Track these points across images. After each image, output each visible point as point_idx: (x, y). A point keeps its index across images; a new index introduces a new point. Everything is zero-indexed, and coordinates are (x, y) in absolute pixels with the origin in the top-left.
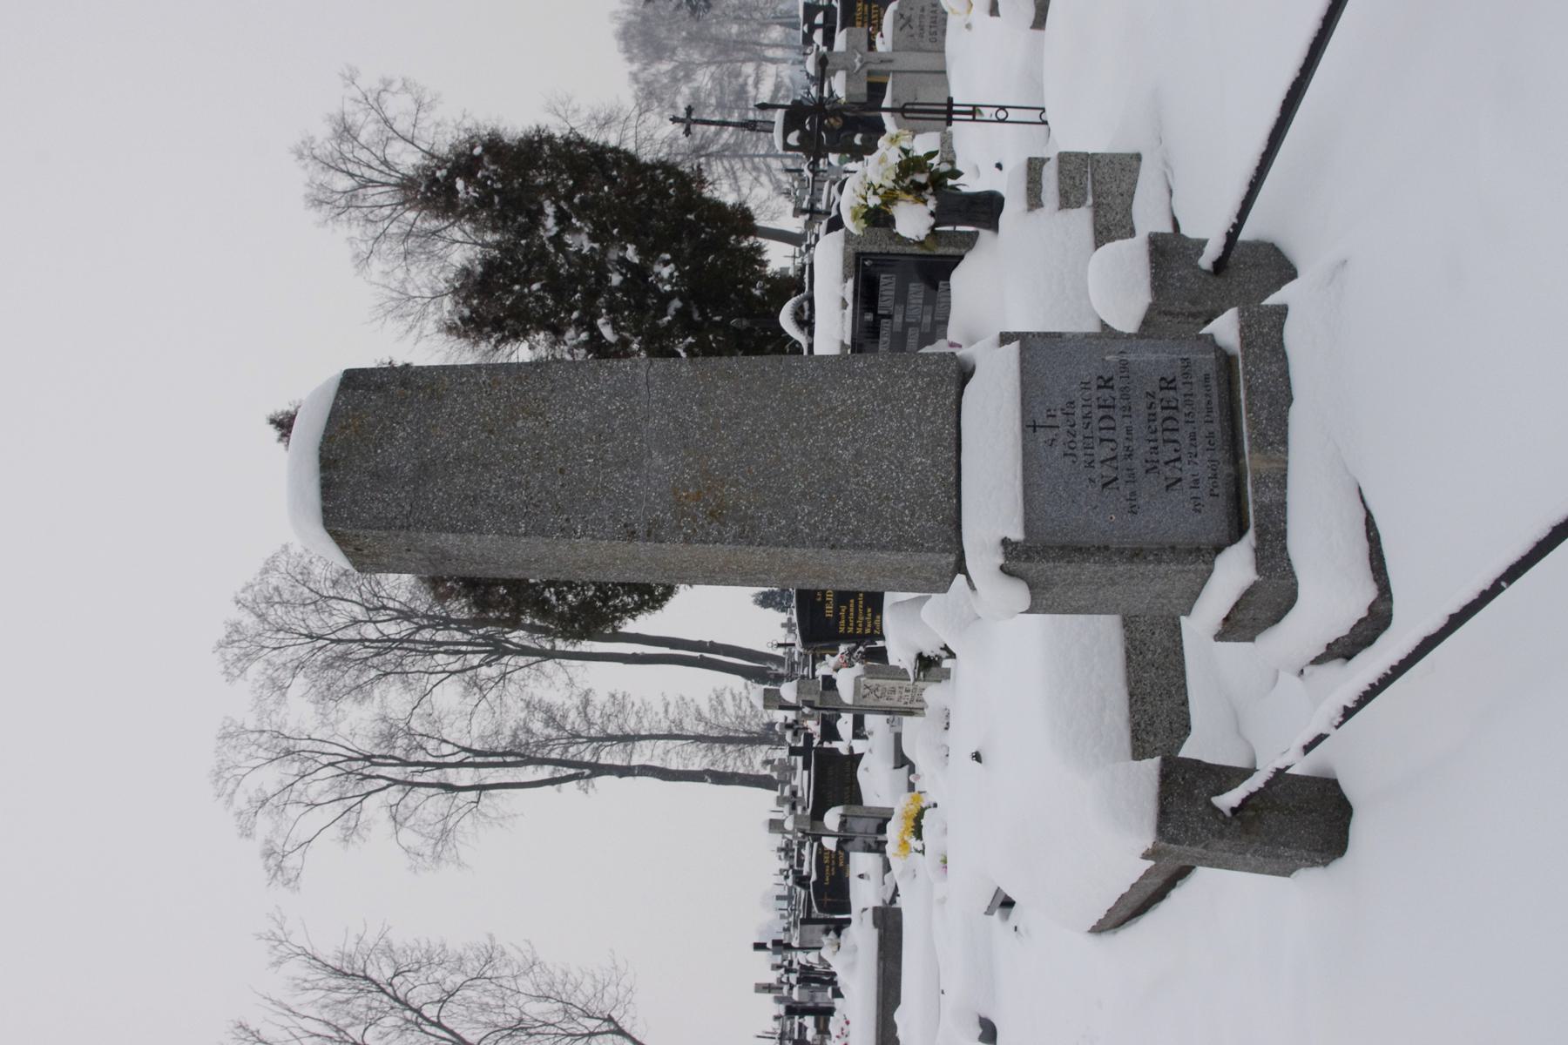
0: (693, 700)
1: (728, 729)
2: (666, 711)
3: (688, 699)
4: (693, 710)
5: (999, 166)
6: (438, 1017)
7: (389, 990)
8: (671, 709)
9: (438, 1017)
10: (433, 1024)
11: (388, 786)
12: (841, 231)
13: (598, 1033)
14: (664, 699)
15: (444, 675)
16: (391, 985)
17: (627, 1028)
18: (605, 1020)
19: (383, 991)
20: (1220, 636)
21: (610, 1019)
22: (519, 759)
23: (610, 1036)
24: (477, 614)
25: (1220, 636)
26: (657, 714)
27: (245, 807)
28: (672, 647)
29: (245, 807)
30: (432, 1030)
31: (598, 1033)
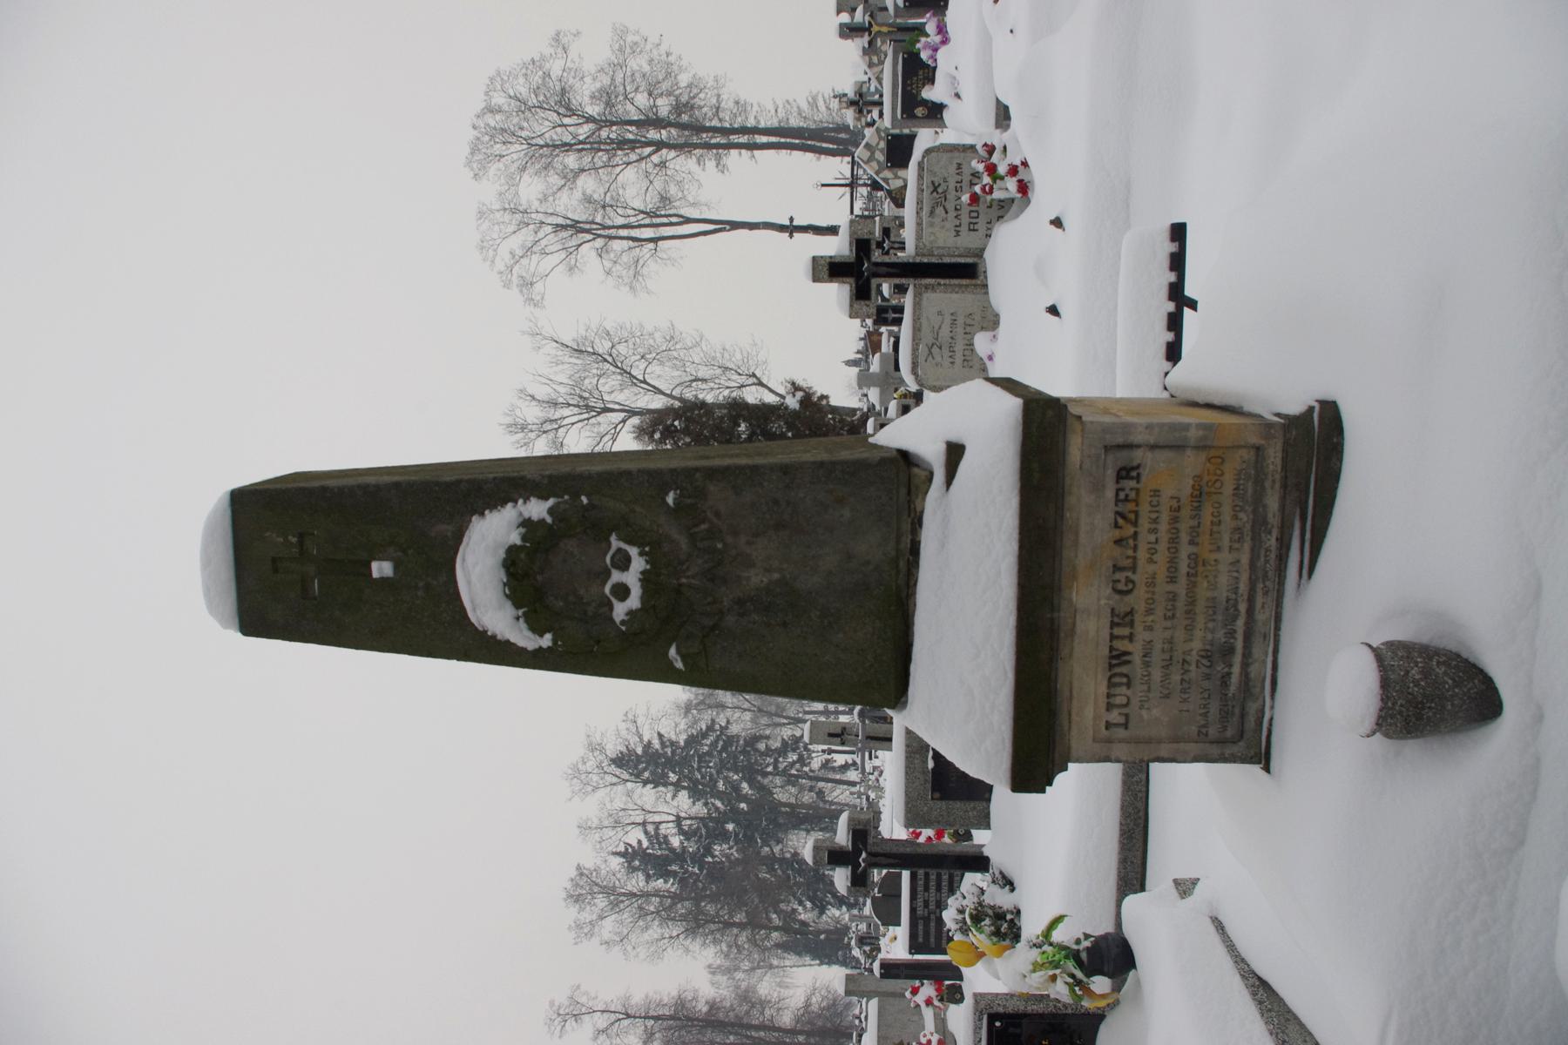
0: (795, 101)
1: (821, 122)
2: (776, 111)
3: (791, 100)
4: (795, 109)
5: (1053, 310)
6: (644, 377)
7: (610, 359)
8: (779, 110)
9: (644, 377)
10: (641, 382)
11: (594, 239)
12: (962, 916)
13: (747, 385)
14: (775, 102)
15: (624, 166)
16: (611, 355)
17: (765, 382)
18: (750, 376)
19: (605, 360)
20: (1196, 311)
21: (754, 375)
22: (681, 220)
23: (754, 387)
24: (689, 851)
25: (1196, 311)
26: (769, 111)
27: (503, 269)
28: (781, 136)
29: (503, 269)
30: (642, 385)
31: (747, 385)
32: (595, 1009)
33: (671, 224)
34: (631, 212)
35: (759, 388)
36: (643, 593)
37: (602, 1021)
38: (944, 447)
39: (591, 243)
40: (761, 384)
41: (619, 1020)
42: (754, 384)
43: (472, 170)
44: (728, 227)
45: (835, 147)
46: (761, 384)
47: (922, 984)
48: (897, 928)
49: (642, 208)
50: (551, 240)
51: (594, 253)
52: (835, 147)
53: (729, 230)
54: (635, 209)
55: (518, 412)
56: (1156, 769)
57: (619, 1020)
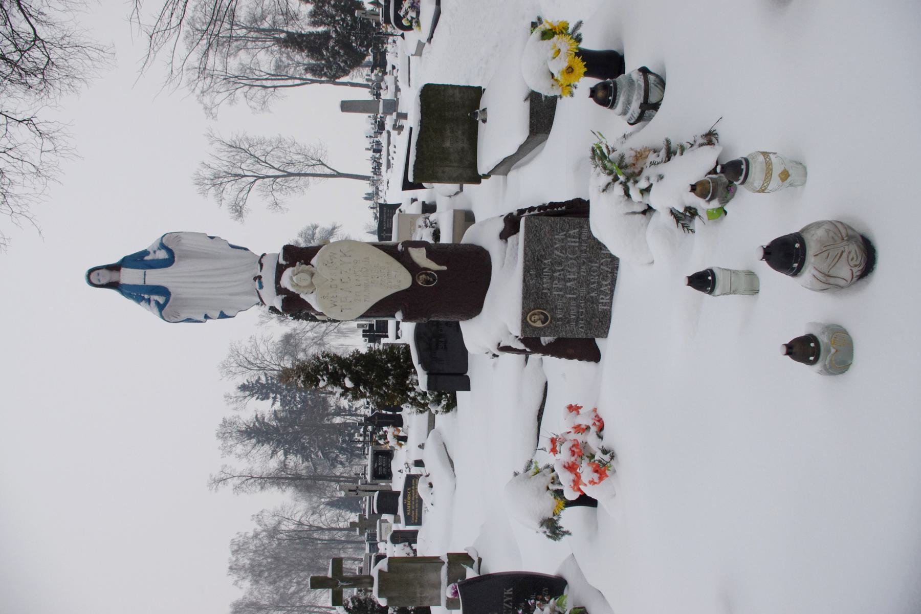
10: (264, 162)
11: (244, 86)
17: (325, 163)
21: (320, 161)
32: (235, 475)
33: (282, 79)
34: (263, 74)
35: (323, 166)
36: (283, 305)
37: (237, 481)
38: (405, 112)
39: (242, 88)
40: (323, 164)
41: (247, 480)
42: (320, 164)
43: (203, 99)
44: (309, 82)
45: (391, 413)
46: (323, 164)
47: (312, 3)
48: (399, 524)
49: (269, 72)
50: (219, 85)
51: (242, 95)
52: (391, 413)
53: (310, 83)
54: (265, 73)
55: (201, 174)
56: (457, 392)
57: (247, 480)
